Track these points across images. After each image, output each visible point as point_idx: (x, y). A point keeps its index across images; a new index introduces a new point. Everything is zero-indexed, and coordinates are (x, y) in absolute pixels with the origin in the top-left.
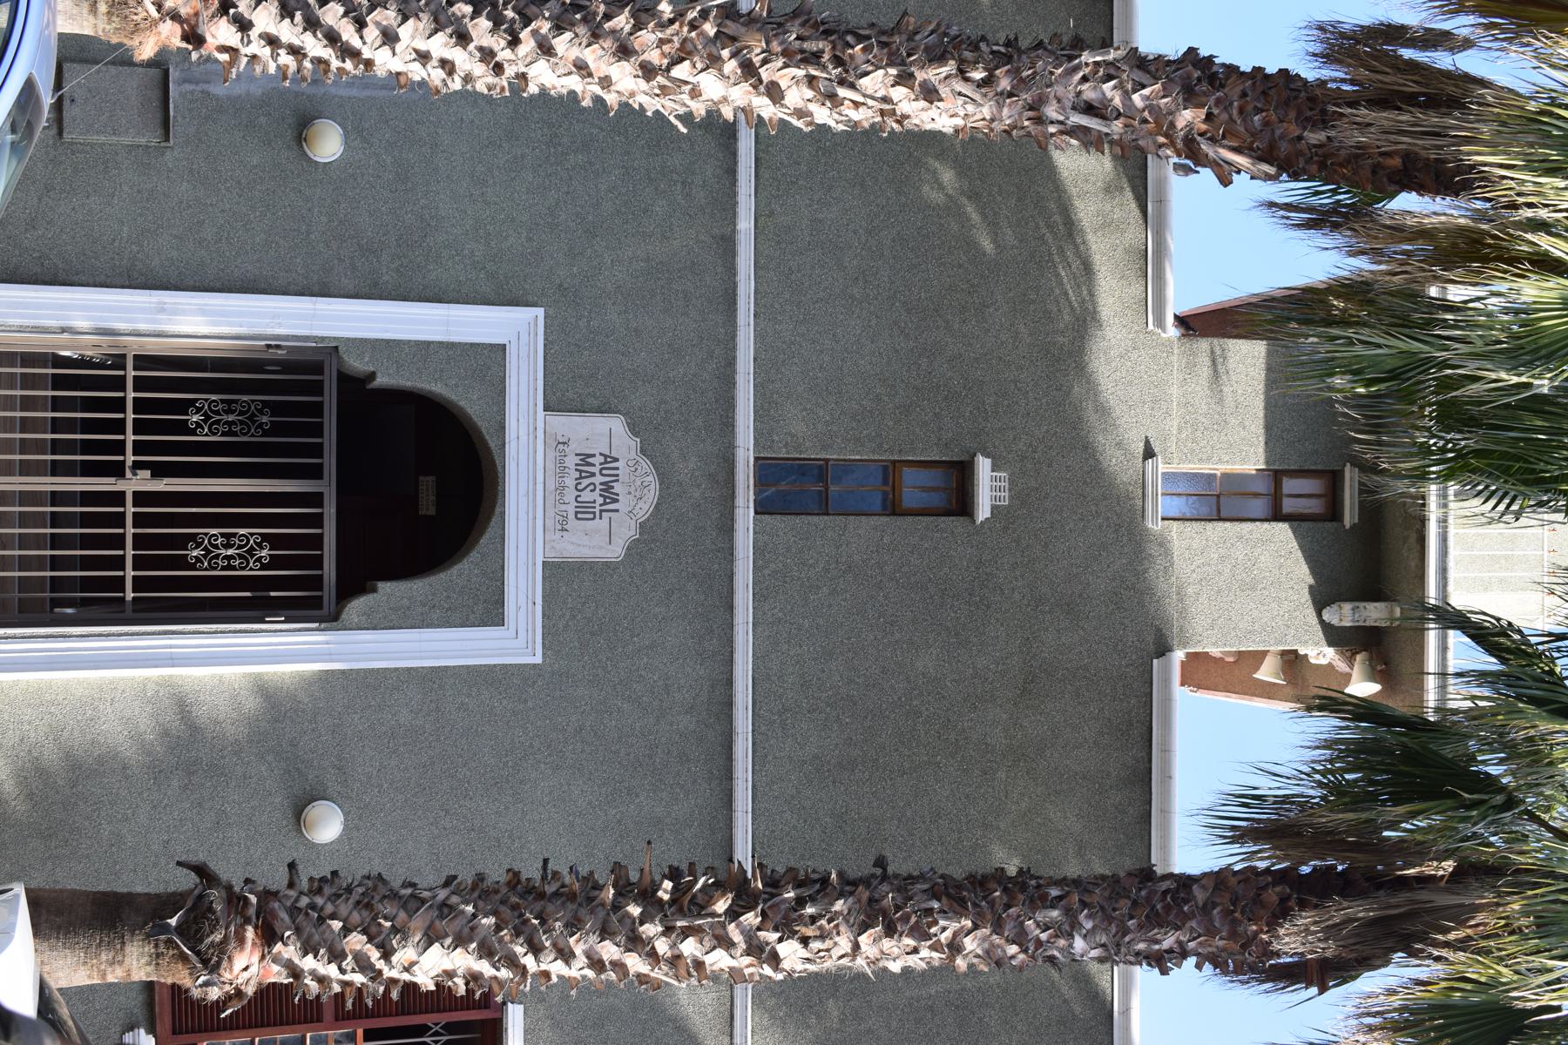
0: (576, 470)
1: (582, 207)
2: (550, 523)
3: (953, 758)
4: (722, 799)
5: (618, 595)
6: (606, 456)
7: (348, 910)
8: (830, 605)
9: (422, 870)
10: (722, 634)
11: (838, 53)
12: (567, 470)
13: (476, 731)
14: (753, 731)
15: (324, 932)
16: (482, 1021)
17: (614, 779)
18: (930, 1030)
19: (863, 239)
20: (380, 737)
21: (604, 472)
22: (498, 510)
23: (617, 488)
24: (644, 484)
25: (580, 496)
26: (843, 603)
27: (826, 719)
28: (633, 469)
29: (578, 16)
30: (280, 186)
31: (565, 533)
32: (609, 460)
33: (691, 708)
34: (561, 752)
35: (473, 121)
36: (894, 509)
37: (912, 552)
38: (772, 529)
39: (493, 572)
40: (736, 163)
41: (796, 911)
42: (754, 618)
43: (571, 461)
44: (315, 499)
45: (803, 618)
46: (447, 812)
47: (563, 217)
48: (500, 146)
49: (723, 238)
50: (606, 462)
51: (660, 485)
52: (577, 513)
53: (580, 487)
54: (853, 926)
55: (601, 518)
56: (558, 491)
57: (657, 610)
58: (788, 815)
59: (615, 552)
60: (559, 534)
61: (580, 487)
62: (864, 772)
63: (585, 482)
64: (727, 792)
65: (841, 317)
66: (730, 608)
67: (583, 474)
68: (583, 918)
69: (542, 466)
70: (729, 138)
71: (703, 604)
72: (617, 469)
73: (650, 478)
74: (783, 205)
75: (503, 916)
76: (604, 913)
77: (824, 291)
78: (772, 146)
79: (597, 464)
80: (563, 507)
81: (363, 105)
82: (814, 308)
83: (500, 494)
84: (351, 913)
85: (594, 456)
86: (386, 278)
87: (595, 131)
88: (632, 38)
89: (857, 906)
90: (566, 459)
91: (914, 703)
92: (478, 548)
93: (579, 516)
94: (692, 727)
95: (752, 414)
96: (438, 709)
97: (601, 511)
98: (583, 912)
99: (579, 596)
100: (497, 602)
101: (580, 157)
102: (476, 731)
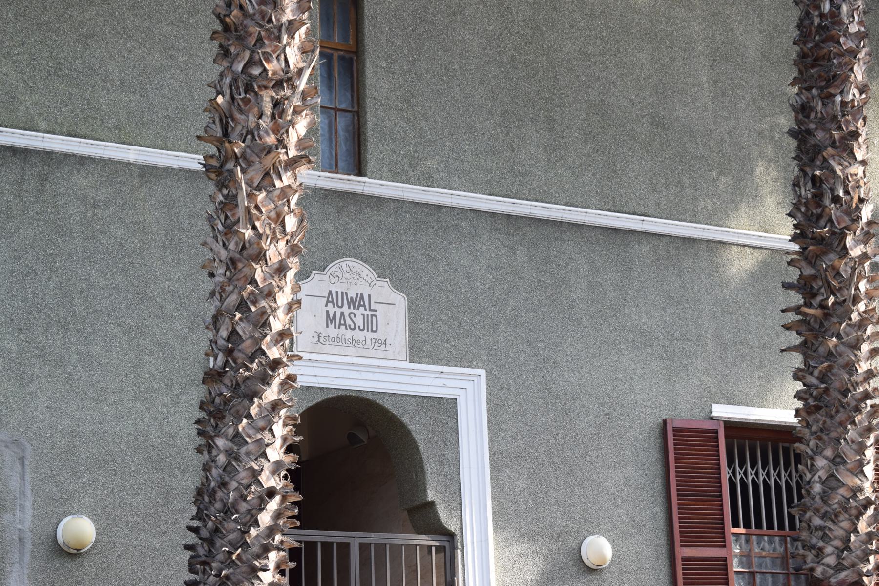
0: (339, 328)
1: (120, 303)
2: (380, 354)
3: (544, 34)
4: (575, 232)
5: (431, 302)
6: (328, 302)
7: (839, 529)
8: (435, 121)
9: (626, 476)
10: (457, 216)
11: (271, 84)
12: (340, 336)
13: (531, 427)
14: (528, 200)
15: (855, 547)
16: (726, 437)
17: (562, 319)
18: (729, 85)
19: (135, 44)
20: (536, 504)
21: (340, 304)
22: (370, 397)
23: (352, 294)
24: (348, 270)
25: (359, 327)
26: (433, 110)
27: (518, 137)
28: (337, 279)
29: (253, 309)
30: (115, 574)
31: (387, 342)
32: (330, 299)
33: (511, 249)
34: (544, 360)
35: (48, 397)
36: (353, 52)
37: (393, 43)
38: (378, 164)
39: (417, 405)
40: (74, 155)
41: (842, 205)
42: (445, 188)
43: (332, 331)
44: (364, 548)
45: (444, 146)
46: (587, 454)
47: (130, 321)
48: (70, 374)
49: (141, 176)
50: (332, 302)
51: (347, 256)
52: (372, 331)
53: (352, 327)
54: (850, 164)
55: (375, 311)
56: (356, 345)
57: (441, 270)
58: (586, 179)
59: (400, 300)
60: (389, 347)
61: (352, 327)
62: (556, 111)
63: (349, 322)
64: (570, 227)
65: (204, 76)
66: (439, 207)
67: (343, 322)
68: (845, 362)
69: (351, 358)
70: (52, 159)
71: (437, 231)
72: (337, 292)
73: (343, 264)
74: (109, 116)
75: (843, 419)
76: (841, 346)
77: (183, 89)
78: (56, 119)
79: (334, 309)
80: (368, 341)
81: (40, 497)
82: (198, 99)
83: (358, 394)
84: (842, 528)
85: (328, 311)
86: (189, 483)
87: (52, 285)
88: (269, 264)
89: (837, 158)
90: (331, 337)
91: (506, 60)
92: (399, 416)
93: (374, 329)
94: (525, 250)
95: (396, 184)
96: (516, 457)
97: (370, 310)
98: (841, 361)
99: (433, 334)
100: (439, 403)
101: (76, 300)
102: (531, 427)
